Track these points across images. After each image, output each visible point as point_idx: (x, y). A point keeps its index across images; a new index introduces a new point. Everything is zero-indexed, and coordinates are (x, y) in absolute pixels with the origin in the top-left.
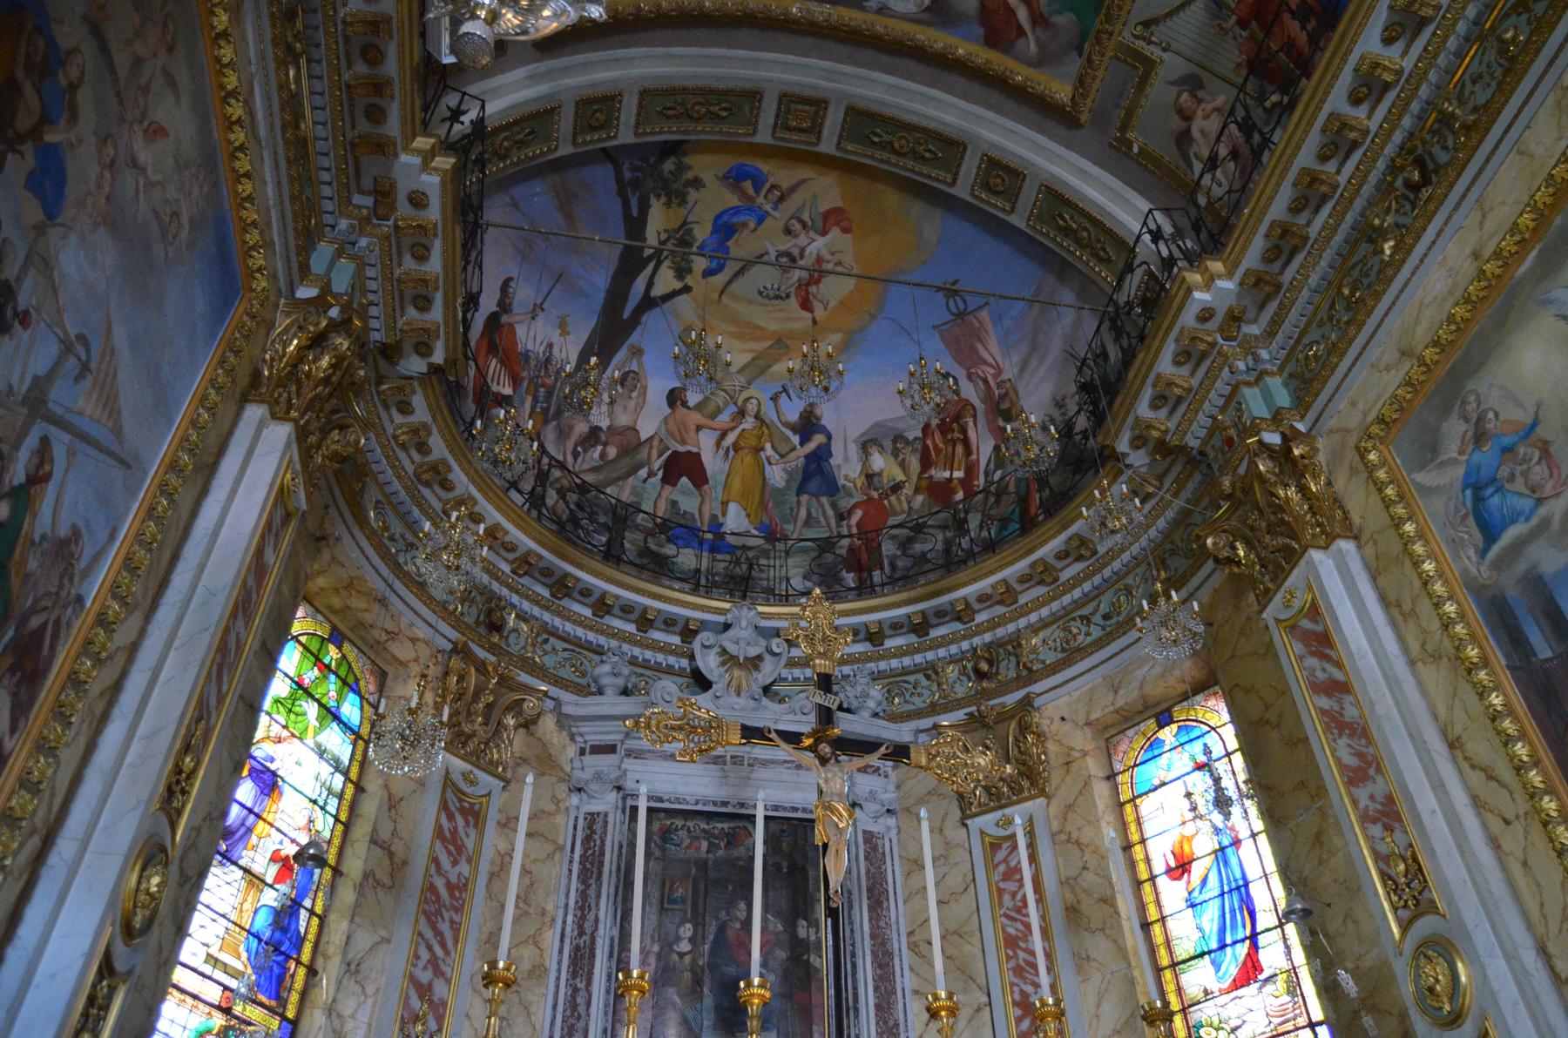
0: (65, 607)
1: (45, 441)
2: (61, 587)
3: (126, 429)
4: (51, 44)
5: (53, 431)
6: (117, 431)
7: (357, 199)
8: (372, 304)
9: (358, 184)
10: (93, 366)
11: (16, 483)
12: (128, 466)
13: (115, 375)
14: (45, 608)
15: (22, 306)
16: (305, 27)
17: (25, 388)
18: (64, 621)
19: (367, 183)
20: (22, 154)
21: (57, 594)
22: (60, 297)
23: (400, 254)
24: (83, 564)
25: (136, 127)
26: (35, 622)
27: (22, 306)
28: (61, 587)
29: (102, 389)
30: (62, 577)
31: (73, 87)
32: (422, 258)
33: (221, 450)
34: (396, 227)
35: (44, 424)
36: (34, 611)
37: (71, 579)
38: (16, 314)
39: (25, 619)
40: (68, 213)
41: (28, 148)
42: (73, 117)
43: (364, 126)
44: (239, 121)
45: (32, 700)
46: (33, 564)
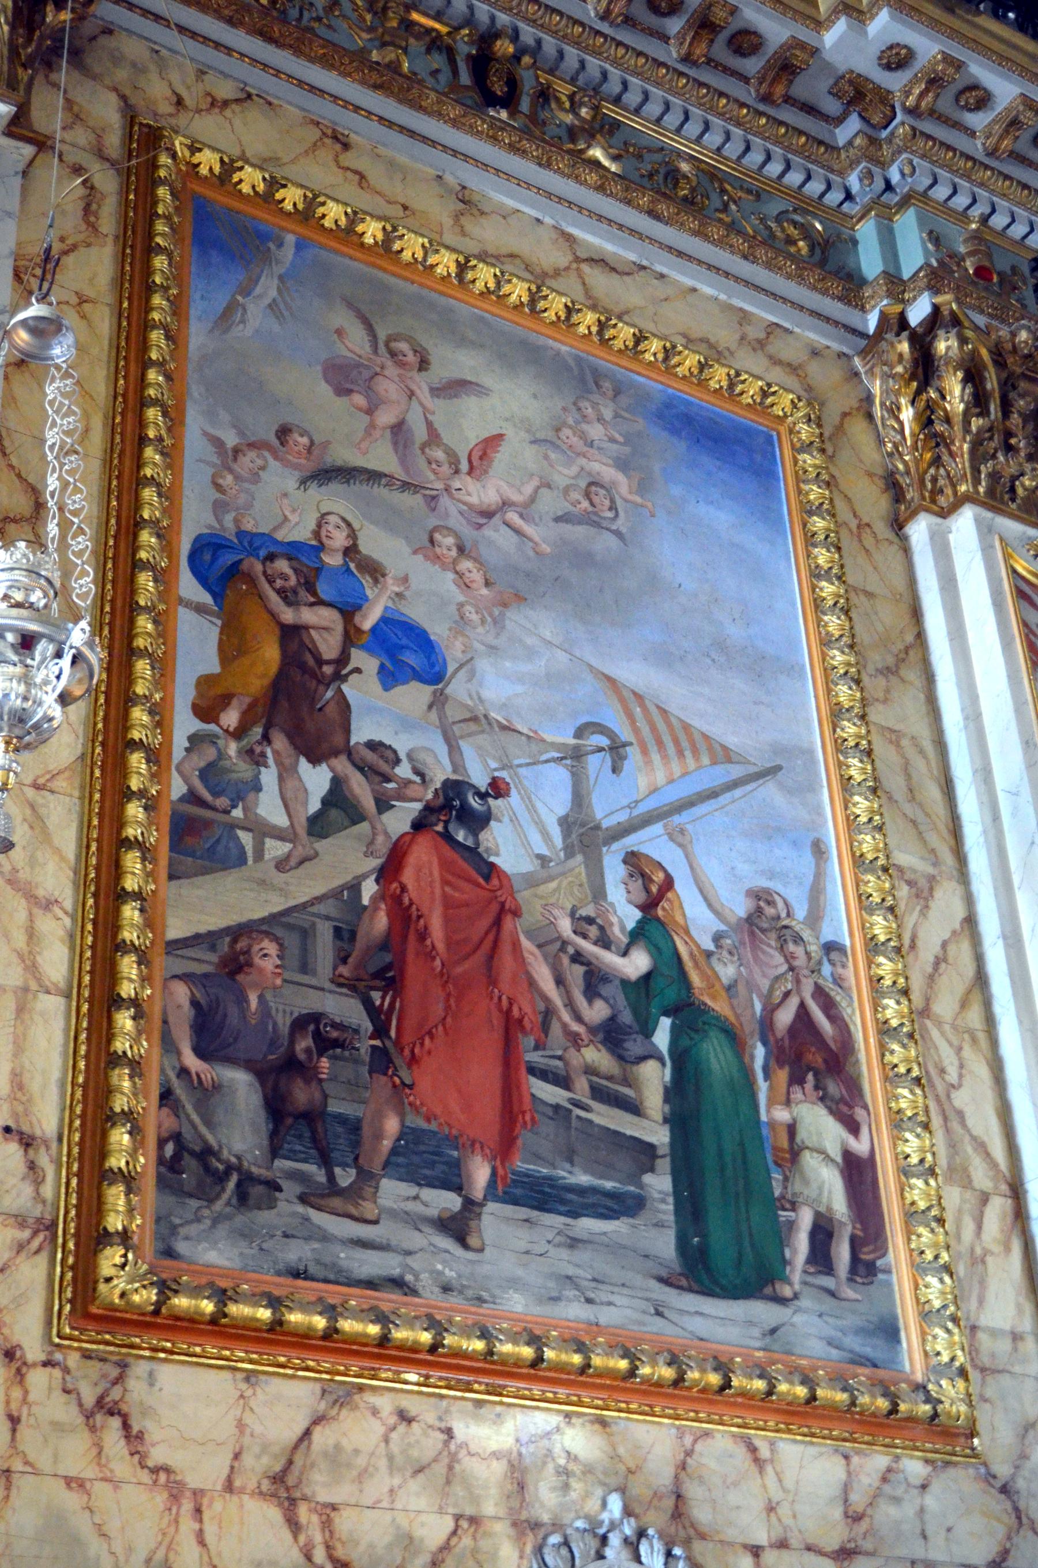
0: (816, 971)
1: (633, 860)
2: (789, 958)
3: (732, 741)
4: (293, 551)
5: (631, 842)
6: (725, 755)
7: (843, 134)
8: (985, 220)
9: (826, 118)
10: (625, 734)
11: (631, 925)
12: (773, 771)
13: (664, 712)
14: (787, 994)
15: (481, 782)
16: (573, 81)
17: (558, 841)
18: (829, 985)
19: (832, 106)
20: (358, 670)
21: (792, 969)
22: (519, 727)
23: (957, 125)
24: (801, 912)
25: (457, 484)
26: (785, 1017)
27: (481, 782)
28: (789, 958)
29: (660, 743)
30: (782, 949)
31: (350, 551)
32: (983, 100)
33: (916, 613)
34: (913, 112)
35: (615, 846)
36: (771, 1010)
37: (798, 939)
38: (483, 796)
39: (766, 1024)
40: (453, 652)
41: (359, 658)
42: (375, 571)
43: (752, 65)
44: (569, 310)
45: (854, 1087)
46: (727, 972)
